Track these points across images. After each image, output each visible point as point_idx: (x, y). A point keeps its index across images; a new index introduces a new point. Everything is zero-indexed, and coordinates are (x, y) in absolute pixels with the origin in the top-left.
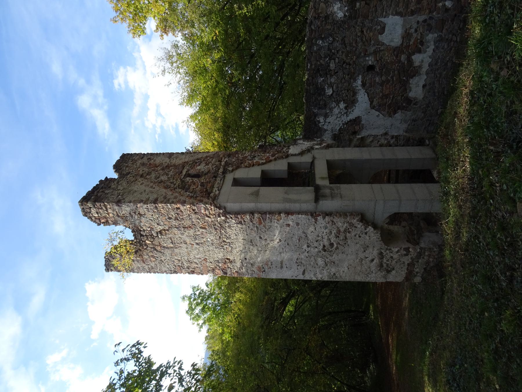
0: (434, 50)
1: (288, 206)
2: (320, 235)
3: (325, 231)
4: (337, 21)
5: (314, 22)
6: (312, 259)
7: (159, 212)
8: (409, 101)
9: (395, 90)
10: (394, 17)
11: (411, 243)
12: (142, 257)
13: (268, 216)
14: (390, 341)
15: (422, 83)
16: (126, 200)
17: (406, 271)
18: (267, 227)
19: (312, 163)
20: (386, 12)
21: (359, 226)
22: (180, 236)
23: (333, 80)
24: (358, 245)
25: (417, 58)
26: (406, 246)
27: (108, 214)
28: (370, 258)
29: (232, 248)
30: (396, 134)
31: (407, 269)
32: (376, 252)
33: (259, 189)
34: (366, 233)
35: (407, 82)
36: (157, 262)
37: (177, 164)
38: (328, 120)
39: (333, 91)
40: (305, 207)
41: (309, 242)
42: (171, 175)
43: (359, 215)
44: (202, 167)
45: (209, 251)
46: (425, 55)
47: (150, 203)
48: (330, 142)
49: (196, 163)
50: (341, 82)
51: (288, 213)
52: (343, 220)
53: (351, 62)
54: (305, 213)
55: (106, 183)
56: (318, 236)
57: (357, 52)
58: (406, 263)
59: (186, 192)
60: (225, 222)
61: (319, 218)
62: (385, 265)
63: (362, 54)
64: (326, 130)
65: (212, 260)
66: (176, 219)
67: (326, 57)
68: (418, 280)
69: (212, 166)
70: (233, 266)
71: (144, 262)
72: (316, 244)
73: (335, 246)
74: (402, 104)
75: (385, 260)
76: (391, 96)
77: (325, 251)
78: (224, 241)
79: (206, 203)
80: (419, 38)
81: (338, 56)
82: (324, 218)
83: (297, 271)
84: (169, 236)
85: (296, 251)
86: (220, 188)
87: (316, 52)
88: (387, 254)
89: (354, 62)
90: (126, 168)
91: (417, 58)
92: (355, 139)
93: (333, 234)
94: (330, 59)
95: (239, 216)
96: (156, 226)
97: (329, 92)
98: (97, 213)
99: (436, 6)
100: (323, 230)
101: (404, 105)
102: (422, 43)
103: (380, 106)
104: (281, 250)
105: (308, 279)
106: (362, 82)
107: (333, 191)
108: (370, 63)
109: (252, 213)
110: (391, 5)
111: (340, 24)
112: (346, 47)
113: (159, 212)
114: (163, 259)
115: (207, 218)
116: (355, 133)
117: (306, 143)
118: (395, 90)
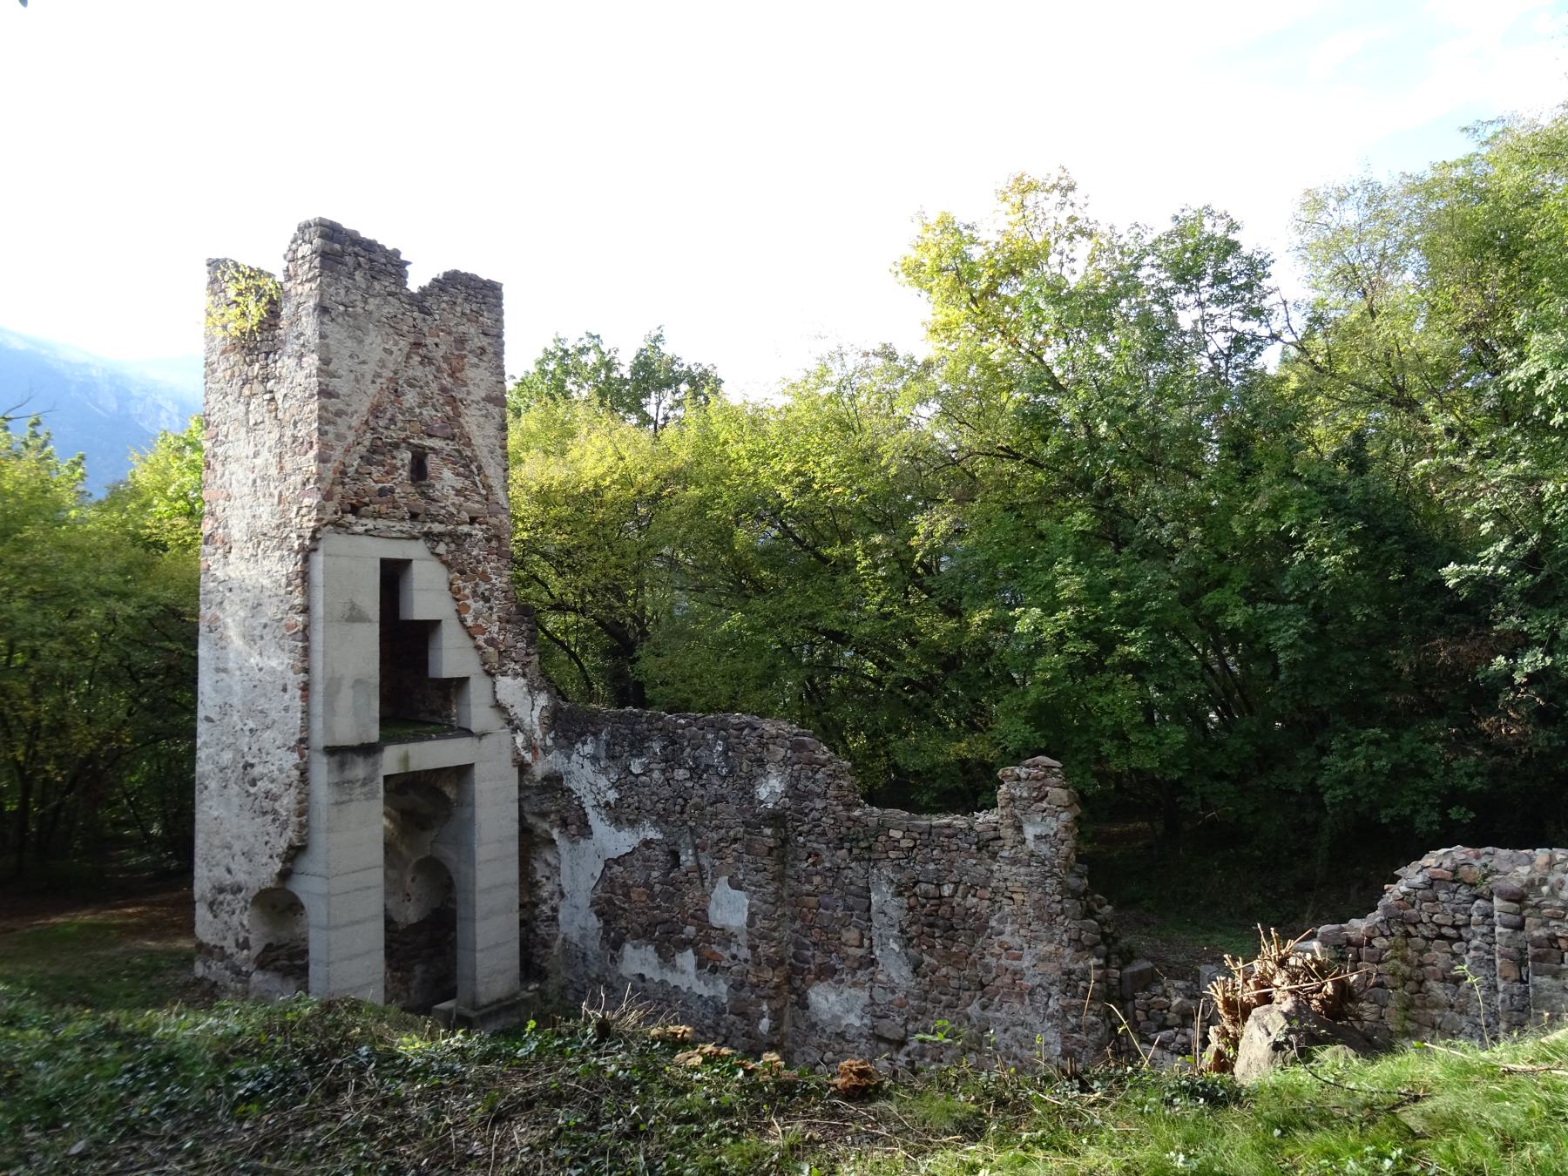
0: (701, 996)
1: (318, 688)
2: (269, 758)
3: (274, 768)
4: (753, 786)
5: (754, 734)
6: (232, 740)
7: (305, 401)
8: (617, 945)
9: (637, 913)
10: (746, 909)
11: (264, 951)
12: (231, 351)
13: (300, 644)
14: (130, 911)
15: (648, 972)
16: (330, 328)
17: (212, 944)
18: (282, 642)
19: (468, 732)
20: (755, 892)
21: (282, 842)
22: (267, 445)
23: (656, 774)
24: (252, 840)
25: (687, 959)
26: (252, 943)
27: (302, 283)
28: (233, 867)
29: (249, 560)
30: (560, 917)
31: (215, 947)
32: (241, 877)
33: (370, 621)
34: (271, 857)
35: (651, 941)
36: (222, 384)
37: (461, 420)
38: (587, 763)
39: (637, 776)
40: (317, 725)
41: (259, 733)
42: (421, 414)
43: (302, 840)
44: (446, 479)
45: (243, 508)
46: (693, 977)
47: (320, 383)
48: (539, 769)
49: (466, 466)
50: (653, 793)
51: (306, 688)
52: (293, 806)
53: (685, 816)
54: (306, 726)
55: (388, 266)
56: (268, 754)
57: (701, 829)
58: (224, 944)
59: (361, 458)
60: (291, 549)
61: (296, 755)
62: (221, 898)
63: (698, 841)
64: (569, 758)
65: (228, 512)
66: (295, 439)
67: (695, 759)
68: (199, 969)
69: (453, 504)
70: (219, 560)
71: (224, 352)
72: (255, 748)
73: (252, 790)
74: (613, 929)
75: (229, 897)
76: (626, 906)
77: (245, 768)
78: (259, 544)
79: (321, 509)
80: (723, 964)
81: (697, 787)
82: (297, 767)
83: (211, 703)
84: (266, 419)
85: (244, 704)
86: (374, 533)
87: (704, 738)
88: (238, 902)
89: (685, 823)
90: (447, 302)
91: (687, 959)
92: (546, 826)
93: (271, 786)
94: (690, 769)
95: (299, 581)
96: (284, 391)
97: (636, 768)
98: (303, 257)
99: (764, 998)
100: (277, 763)
101: (612, 934)
102: (714, 970)
103: (611, 880)
104: (245, 671)
105: (199, 730)
106: (652, 841)
107: (358, 784)
108: (683, 858)
109: (306, 610)
110: (766, 902)
111: (748, 794)
112: (712, 805)
113: (305, 401)
114: (229, 398)
115: (295, 509)
116: (564, 824)
117: (536, 713)
118: (637, 913)
